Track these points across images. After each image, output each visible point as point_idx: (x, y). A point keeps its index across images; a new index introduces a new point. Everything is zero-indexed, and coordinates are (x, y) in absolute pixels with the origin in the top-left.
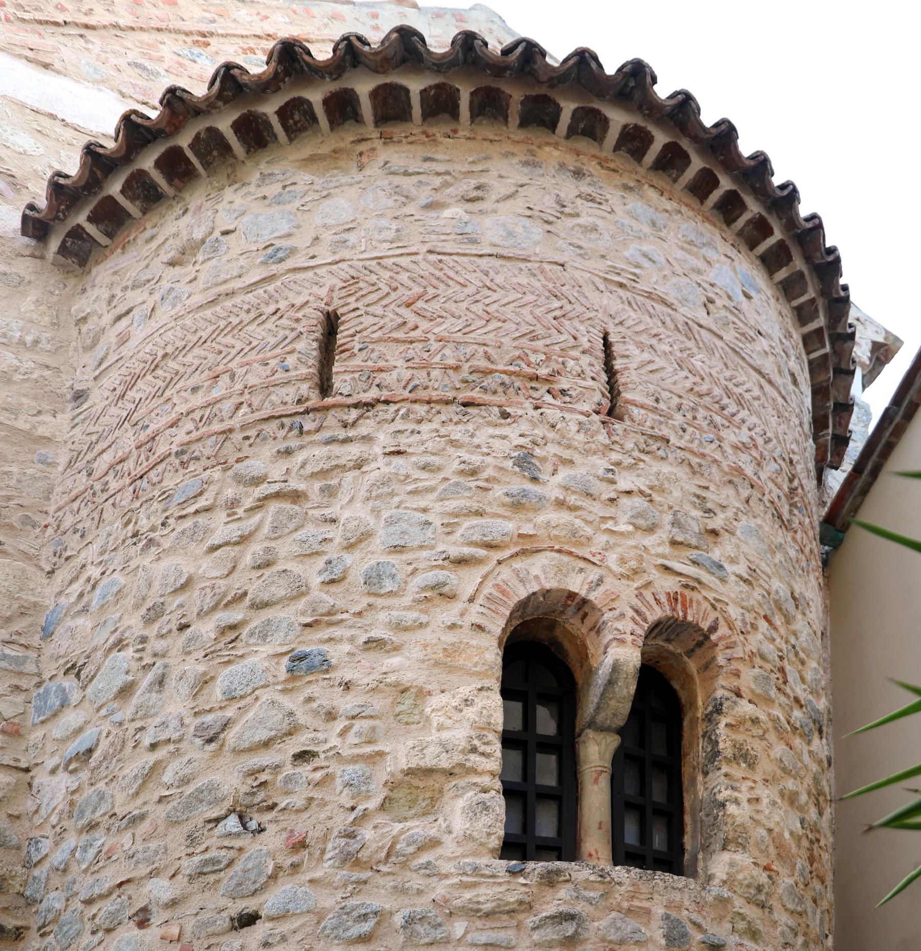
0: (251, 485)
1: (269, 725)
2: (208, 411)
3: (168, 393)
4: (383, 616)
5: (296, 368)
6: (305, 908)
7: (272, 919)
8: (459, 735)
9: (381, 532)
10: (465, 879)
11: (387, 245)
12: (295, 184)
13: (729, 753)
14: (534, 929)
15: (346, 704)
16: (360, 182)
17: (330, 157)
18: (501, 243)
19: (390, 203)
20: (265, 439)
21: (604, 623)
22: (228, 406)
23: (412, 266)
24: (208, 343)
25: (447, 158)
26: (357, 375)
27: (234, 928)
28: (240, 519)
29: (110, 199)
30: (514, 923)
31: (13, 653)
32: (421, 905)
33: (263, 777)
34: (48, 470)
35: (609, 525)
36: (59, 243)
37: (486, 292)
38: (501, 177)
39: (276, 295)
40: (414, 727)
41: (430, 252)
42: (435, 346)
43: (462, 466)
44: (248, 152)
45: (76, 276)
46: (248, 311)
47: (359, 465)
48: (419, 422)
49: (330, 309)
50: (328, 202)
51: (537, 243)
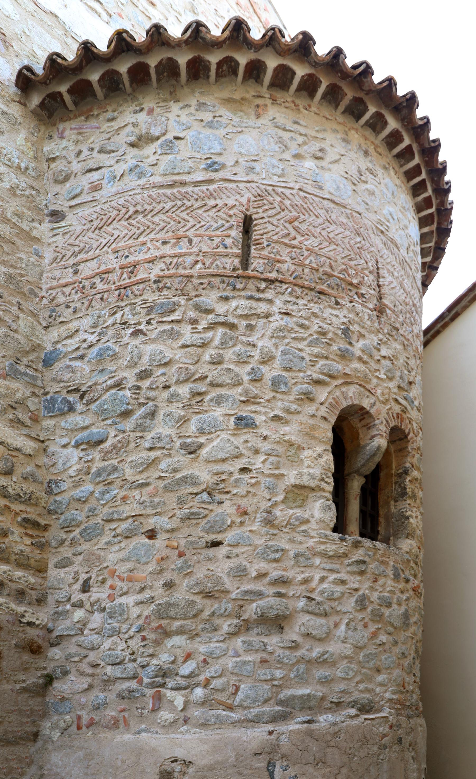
0: (204, 313)
1: (226, 451)
2: (175, 260)
3: (142, 239)
4: (279, 404)
5: (231, 248)
6: (248, 543)
7: (229, 545)
8: (317, 471)
9: (279, 358)
10: (321, 540)
11: (276, 178)
12: (221, 116)
13: (410, 494)
14: (348, 565)
15: (265, 446)
16: (259, 128)
17: (239, 102)
18: (334, 193)
19: (277, 148)
20: (212, 287)
21: (374, 425)
22: (189, 260)
23: (291, 197)
24: (170, 213)
25: (305, 124)
26: (266, 261)
27: (207, 547)
28: (200, 332)
29: (89, 83)
30: (340, 562)
31: (31, 373)
32: (301, 548)
33: (223, 477)
34: (40, 260)
35: (377, 374)
36: (41, 100)
37: (327, 224)
38: (332, 146)
39: (215, 194)
40: (295, 463)
41: (300, 189)
42: (306, 253)
43: (320, 329)
44: (188, 80)
45: (44, 124)
46: (197, 200)
47: (267, 316)
48: (297, 298)
49: (249, 213)
50: (241, 136)
51: (349, 197)
